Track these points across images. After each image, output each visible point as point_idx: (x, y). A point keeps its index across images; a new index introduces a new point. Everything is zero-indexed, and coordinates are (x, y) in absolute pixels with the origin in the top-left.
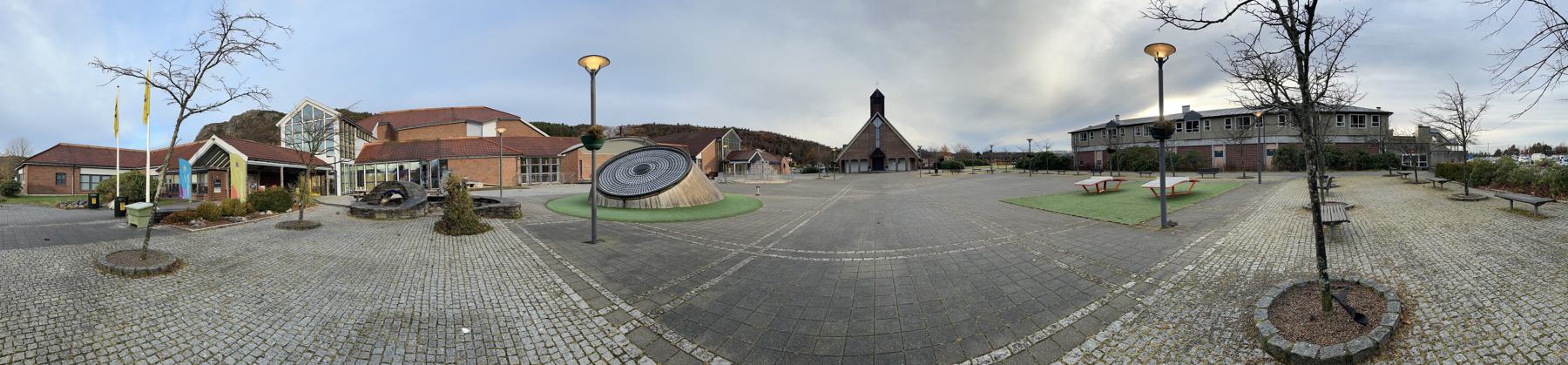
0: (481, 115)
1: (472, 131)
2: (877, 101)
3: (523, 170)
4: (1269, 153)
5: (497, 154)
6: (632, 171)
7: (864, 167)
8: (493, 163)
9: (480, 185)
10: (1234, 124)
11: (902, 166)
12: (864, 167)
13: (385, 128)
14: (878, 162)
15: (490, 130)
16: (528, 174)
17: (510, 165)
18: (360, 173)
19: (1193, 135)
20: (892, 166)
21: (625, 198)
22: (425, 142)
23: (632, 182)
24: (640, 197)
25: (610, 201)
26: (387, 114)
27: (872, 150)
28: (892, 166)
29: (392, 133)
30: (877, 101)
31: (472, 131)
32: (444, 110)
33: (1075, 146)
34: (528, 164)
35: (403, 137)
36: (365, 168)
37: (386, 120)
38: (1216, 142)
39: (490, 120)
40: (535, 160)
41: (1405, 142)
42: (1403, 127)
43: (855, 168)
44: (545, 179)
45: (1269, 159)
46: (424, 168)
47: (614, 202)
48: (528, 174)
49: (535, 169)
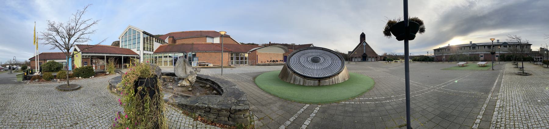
0: (214, 34)
1: (209, 40)
2: (363, 36)
3: (232, 59)
4: (497, 56)
5: (220, 51)
6: (310, 59)
7: (360, 60)
8: (218, 55)
9: (211, 65)
10: (486, 47)
11: (373, 60)
12: (360, 60)
13: (171, 39)
14: (364, 58)
15: (217, 40)
16: (234, 61)
17: (226, 56)
18: (156, 58)
19: (474, 50)
20: (370, 59)
21: (319, 79)
22: (187, 44)
23: (309, 66)
24: (329, 77)
25: (308, 81)
26: (174, 33)
27: (362, 54)
28: (370, 59)
29: (174, 41)
30: (363, 36)
31: (209, 40)
32: (197, 32)
33: (435, 54)
34: (234, 56)
35: (178, 42)
36: (158, 55)
37: (172, 35)
38: (482, 52)
39: (217, 36)
40: (237, 54)
41: (536, 53)
42: (535, 48)
43: (356, 60)
44: (242, 63)
45: (497, 58)
46: (186, 56)
47: (312, 82)
48: (234, 61)
49: (238, 59)
